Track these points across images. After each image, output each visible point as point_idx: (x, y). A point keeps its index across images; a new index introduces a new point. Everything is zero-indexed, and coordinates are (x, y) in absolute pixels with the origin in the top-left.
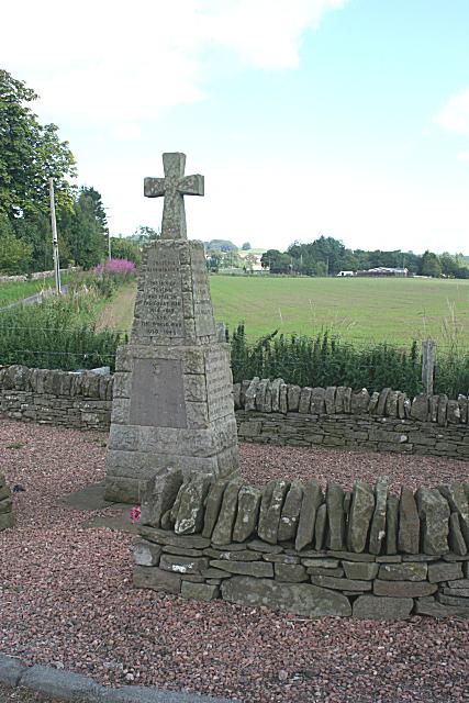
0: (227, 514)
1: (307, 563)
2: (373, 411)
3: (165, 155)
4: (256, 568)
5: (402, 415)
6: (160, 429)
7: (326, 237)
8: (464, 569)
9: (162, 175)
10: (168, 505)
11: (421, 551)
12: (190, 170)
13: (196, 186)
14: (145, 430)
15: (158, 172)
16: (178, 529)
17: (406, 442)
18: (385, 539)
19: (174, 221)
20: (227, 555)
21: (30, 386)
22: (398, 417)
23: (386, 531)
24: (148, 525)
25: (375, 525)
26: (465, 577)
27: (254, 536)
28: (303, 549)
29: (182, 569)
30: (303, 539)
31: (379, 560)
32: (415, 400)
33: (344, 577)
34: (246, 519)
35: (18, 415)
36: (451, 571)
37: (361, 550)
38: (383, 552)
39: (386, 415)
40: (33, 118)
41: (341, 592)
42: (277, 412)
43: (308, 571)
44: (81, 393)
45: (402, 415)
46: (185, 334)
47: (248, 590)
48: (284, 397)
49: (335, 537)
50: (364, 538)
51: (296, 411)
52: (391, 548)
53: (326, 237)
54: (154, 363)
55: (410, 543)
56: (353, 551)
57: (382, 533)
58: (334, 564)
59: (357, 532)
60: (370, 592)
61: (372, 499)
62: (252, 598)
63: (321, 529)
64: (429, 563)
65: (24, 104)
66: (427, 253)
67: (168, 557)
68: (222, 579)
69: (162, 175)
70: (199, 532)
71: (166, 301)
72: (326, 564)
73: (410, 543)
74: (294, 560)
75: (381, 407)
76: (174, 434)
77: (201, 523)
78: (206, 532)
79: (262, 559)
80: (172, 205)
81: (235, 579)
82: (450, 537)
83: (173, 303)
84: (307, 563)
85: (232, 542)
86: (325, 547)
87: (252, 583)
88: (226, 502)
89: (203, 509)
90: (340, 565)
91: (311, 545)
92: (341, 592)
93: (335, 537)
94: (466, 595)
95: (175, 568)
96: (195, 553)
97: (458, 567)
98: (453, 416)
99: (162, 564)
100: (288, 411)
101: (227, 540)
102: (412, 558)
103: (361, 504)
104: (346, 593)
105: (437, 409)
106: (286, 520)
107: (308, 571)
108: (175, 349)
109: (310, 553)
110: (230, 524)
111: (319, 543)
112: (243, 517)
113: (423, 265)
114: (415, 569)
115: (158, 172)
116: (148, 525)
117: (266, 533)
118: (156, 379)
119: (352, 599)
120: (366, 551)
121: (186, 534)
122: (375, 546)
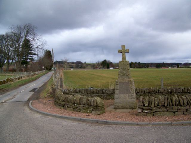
0: (153, 102)
1: (167, 108)
2: (154, 92)
3: (125, 46)
4: (159, 110)
5: (159, 92)
6: (125, 95)
8: (190, 107)
9: (121, 49)
10: (143, 102)
11: (183, 105)
13: (127, 51)
14: (122, 95)
16: (146, 105)
18: (178, 103)
19: (124, 58)
20: (154, 109)
21: (81, 92)
22: (159, 92)
24: (140, 106)
26: (190, 108)
27: (158, 105)
29: (147, 112)
30: (166, 105)
36: (188, 107)
39: (156, 92)
45: (159, 92)
46: (129, 77)
47: (158, 113)
48: (136, 90)
51: (139, 93)
52: (179, 105)
54: (123, 83)
55: (182, 104)
57: (178, 103)
58: (171, 108)
59: (174, 103)
60: (177, 112)
62: (159, 115)
63: (168, 103)
64: (185, 106)
67: (144, 110)
68: (153, 113)
69: (121, 49)
70: (148, 106)
72: (170, 108)
73: (182, 104)
74: (165, 108)
75: (155, 91)
76: (127, 95)
77: (149, 104)
78: (150, 106)
79: (160, 109)
80: (124, 55)
81: (156, 112)
82: (187, 103)
84: (167, 108)
85: (155, 106)
86: (170, 106)
87: (158, 112)
88: (153, 101)
89: (149, 102)
90: (172, 108)
91: (167, 106)
94: (190, 110)
95: (146, 112)
96: (149, 109)
97: (189, 107)
98: (169, 91)
99: (143, 111)
101: (154, 106)
105: (166, 91)
106: (163, 102)
108: (127, 80)
111: (169, 105)
114: (183, 107)
116: (140, 106)
118: (124, 86)
119: (174, 113)
120: (175, 106)
121: (147, 106)
122: (177, 105)
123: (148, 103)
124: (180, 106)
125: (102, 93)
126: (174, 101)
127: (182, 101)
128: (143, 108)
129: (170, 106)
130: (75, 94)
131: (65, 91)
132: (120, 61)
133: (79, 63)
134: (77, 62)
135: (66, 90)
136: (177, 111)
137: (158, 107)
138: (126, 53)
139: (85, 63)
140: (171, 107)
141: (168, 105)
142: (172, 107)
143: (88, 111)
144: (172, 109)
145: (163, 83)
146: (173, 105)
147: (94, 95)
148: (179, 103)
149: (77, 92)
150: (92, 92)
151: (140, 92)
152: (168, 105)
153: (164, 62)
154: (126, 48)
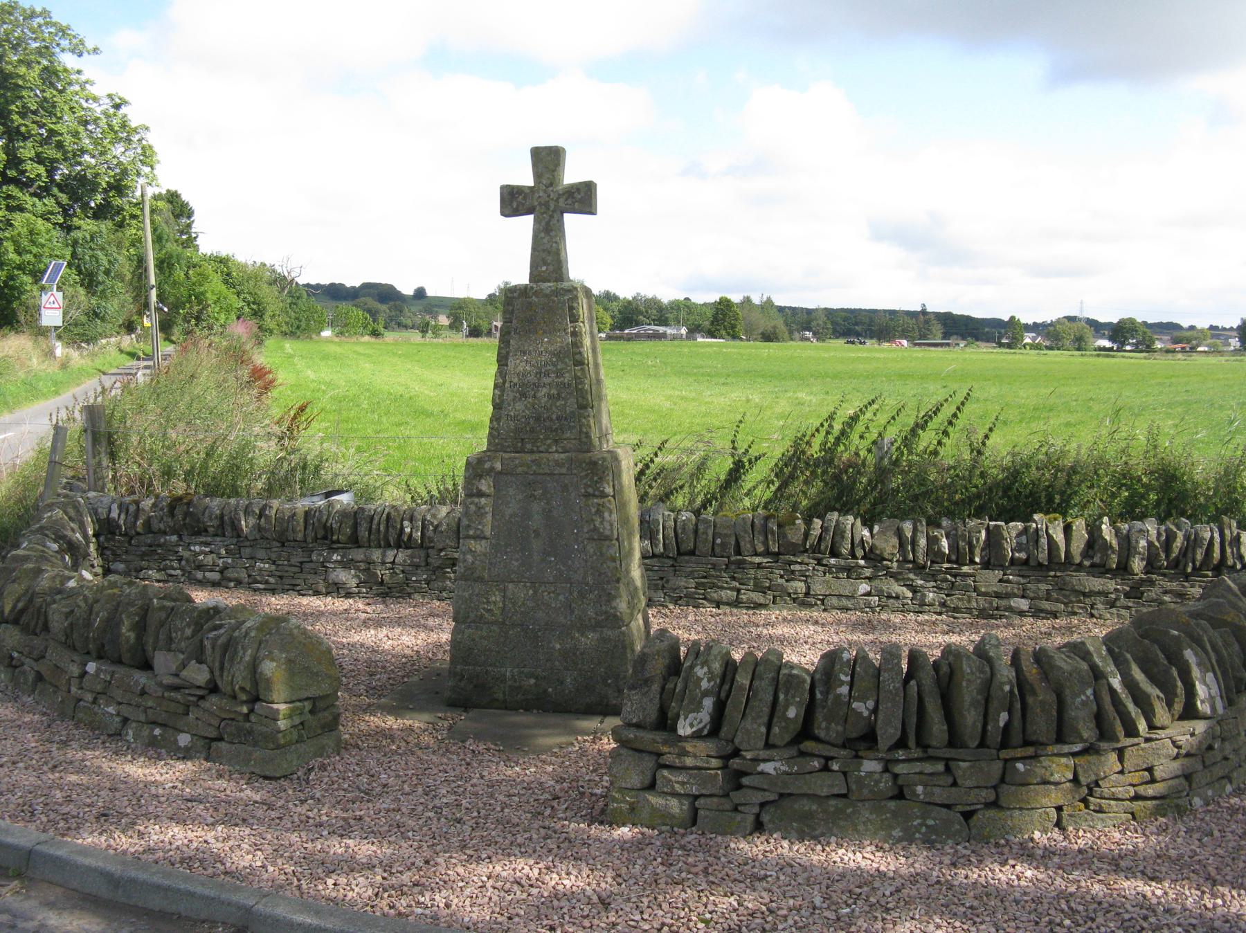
2: (816, 549)
5: (860, 553)
7: (756, 300)
12: (572, 175)
15: (524, 177)
17: (869, 594)
18: (1008, 725)
23: (1010, 714)
25: (994, 704)
27: (805, 732)
28: (890, 749)
30: (888, 732)
31: (1004, 754)
32: (876, 528)
33: (955, 784)
34: (791, 713)
35: (215, 576)
37: (976, 743)
38: (1004, 745)
39: (834, 553)
40: (83, 86)
41: (948, 807)
42: (661, 556)
43: (900, 782)
44: (325, 538)
49: (937, 728)
50: (980, 726)
52: (1016, 738)
53: (756, 300)
56: (967, 747)
57: (1004, 717)
58: (940, 767)
59: (970, 718)
61: (987, 669)
63: (914, 720)
64: (1074, 755)
65: (68, 60)
66: (1012, 318)
68: (762, 805)
71: (546, 380)
72: (928, 768)
78: (724, 731)
79: (826, 768)
83: (557, 385)
84: (900, 769)
86: (922, 744)
90: (948, 769)
91: (901, 743)
92: (948, 807)
93: (937, 728)
100: (679, 554)
102: (1050, 749)
103: (970, 673)
104: (960, 808)
107: (900, 782)
109: (901, 754)
110: (766, 719)
112: (786, 708)
113: (1121, 332)
115: (524, 177)
117: (828, 729)
119: (967, 816)
120: (982, 744)
122: (995, 737)
123: (708, 703)
124: (1027, 743)
125: (398, 546)
126: (967, 699)
127: (1052, 698)
128: (659, 755)
129: (922, 744)
130: (186, 539)
131: (114, 514)
132: (659, 297)
133: (385, 294)
134: (332, 285)
135: (120, 507)
136: (991, 796)
137: (802, 754)
138: (566, 216)
139: (420, 293)
140: (937, 759)
141: (912, 742)
142: (947, 761)
143: (184, 739)
144: (950, 780)
145: (510, 686)
146: (954, 740)
147: (335, 557)
148: (1017, 723)
149: (206, 531)
150: (321, 533)
151: (704, 548)
152: (912, 742)
153: (929, 310)
154: (572, 175)
